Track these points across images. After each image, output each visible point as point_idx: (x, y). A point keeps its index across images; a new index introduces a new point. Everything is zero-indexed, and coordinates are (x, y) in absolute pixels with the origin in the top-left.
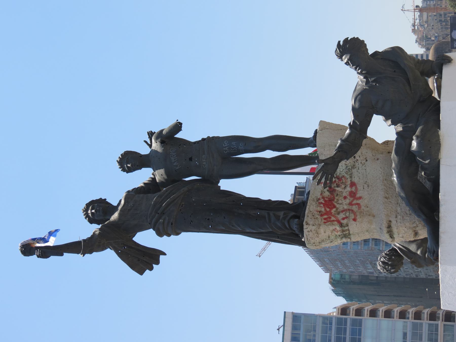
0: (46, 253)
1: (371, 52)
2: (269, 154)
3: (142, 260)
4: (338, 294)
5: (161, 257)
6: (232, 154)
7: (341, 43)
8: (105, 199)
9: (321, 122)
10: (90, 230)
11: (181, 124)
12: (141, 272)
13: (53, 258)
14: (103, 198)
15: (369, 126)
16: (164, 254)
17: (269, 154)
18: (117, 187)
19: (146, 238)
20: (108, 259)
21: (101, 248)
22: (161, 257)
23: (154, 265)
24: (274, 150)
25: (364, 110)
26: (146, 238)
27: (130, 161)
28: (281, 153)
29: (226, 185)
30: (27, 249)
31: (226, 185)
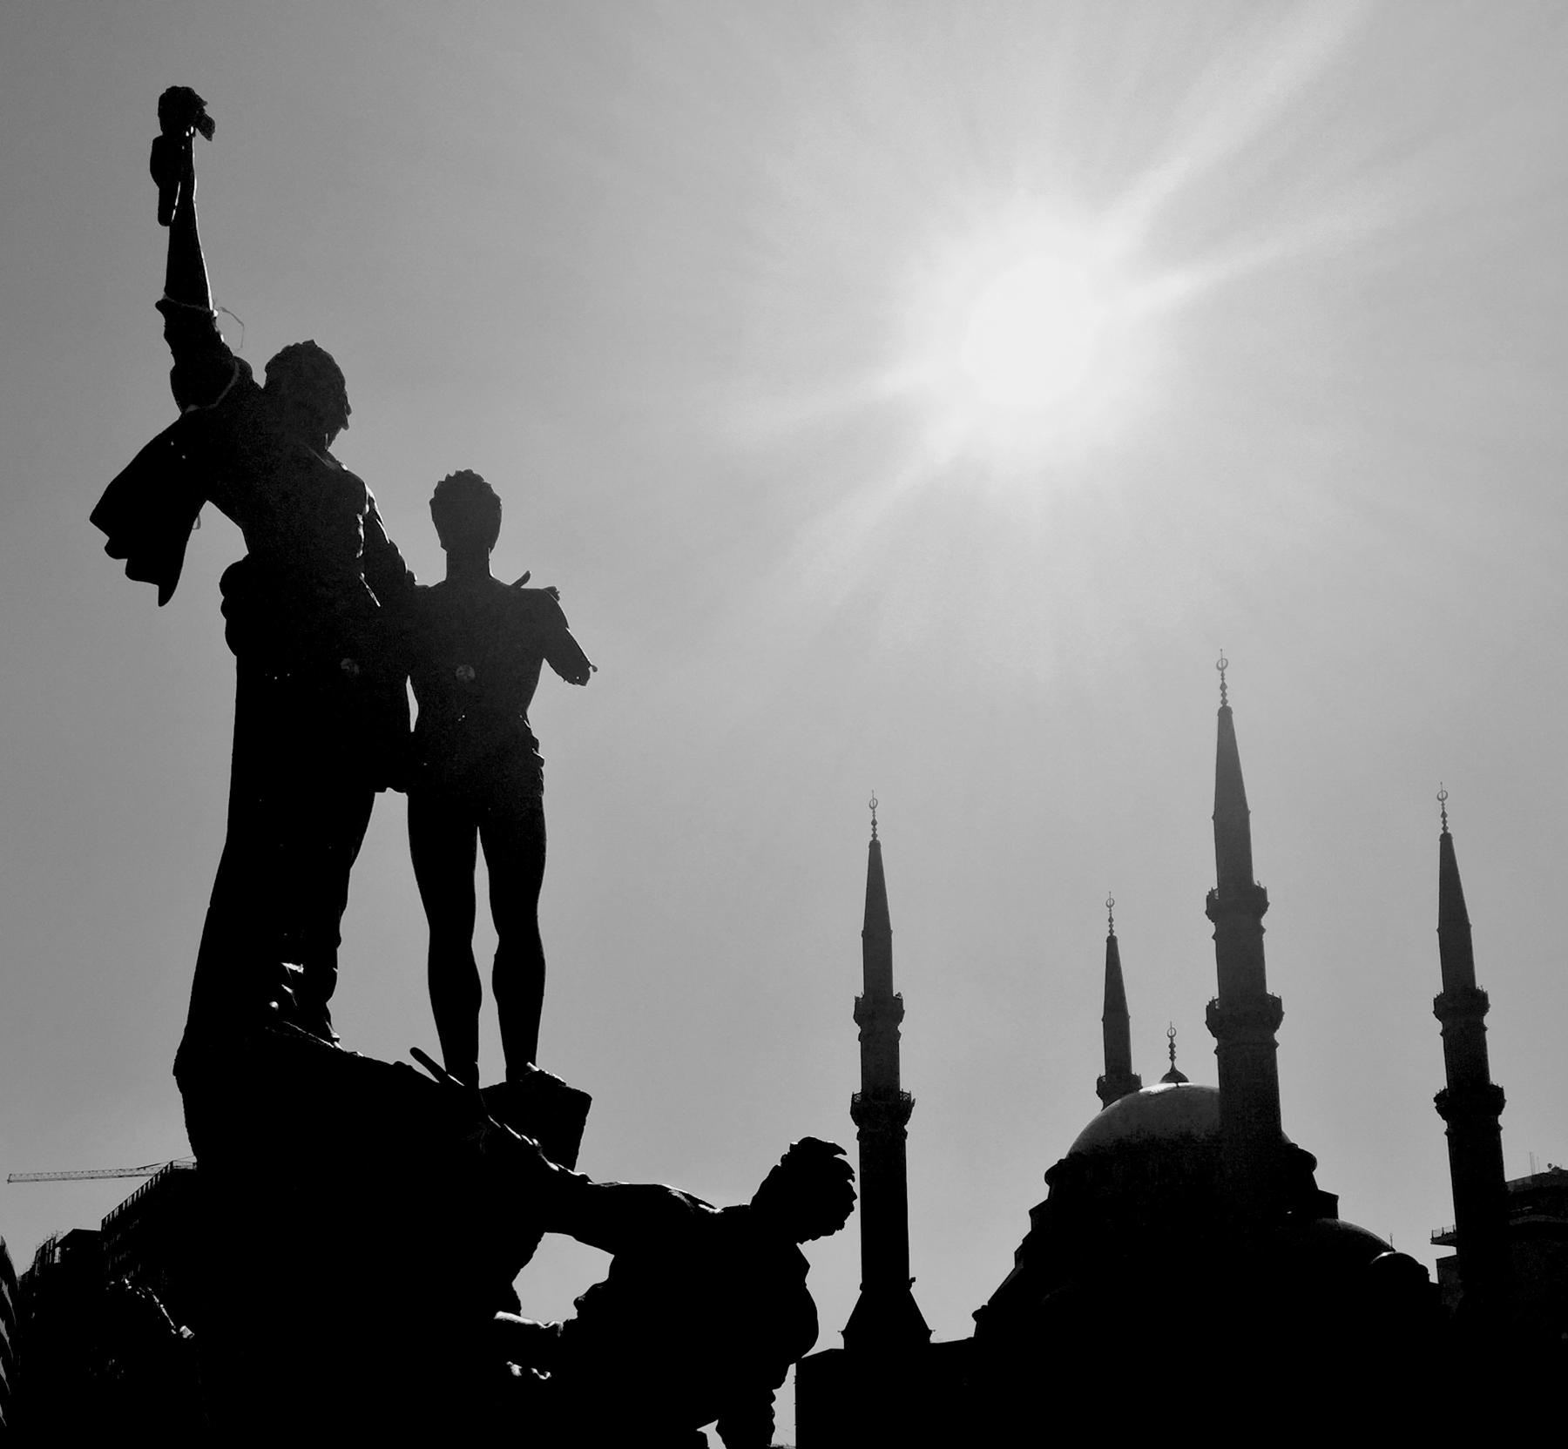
0: (171, 166)
1: (807, 1248)
2: (485, 942)
3: (141, 523)
4: (44, 1253)
5: (153, 590)
6: (487, 823)
7: (839, 1156)
8: (346, 427)
9: (581, 1102)
10: (252, 337)
11: (583, 681)
12: (99, 517)
13: (151, 192)
14: (350, 419)
15: (578, 1239)
16: (164, 598)
17: (485, 942)
18: (390, 464)
19: (216, 542)
20: (142, 404)
21: (182, 384)
22: (153, 590)
23: (1429, 1257)
24: (499, 957)
25: (637, 1221)
26: (216, 542)
27: (466, 510)
28: (493, 966)
29: (390, 811)
30: (182, 113)
31: (390, 811)
